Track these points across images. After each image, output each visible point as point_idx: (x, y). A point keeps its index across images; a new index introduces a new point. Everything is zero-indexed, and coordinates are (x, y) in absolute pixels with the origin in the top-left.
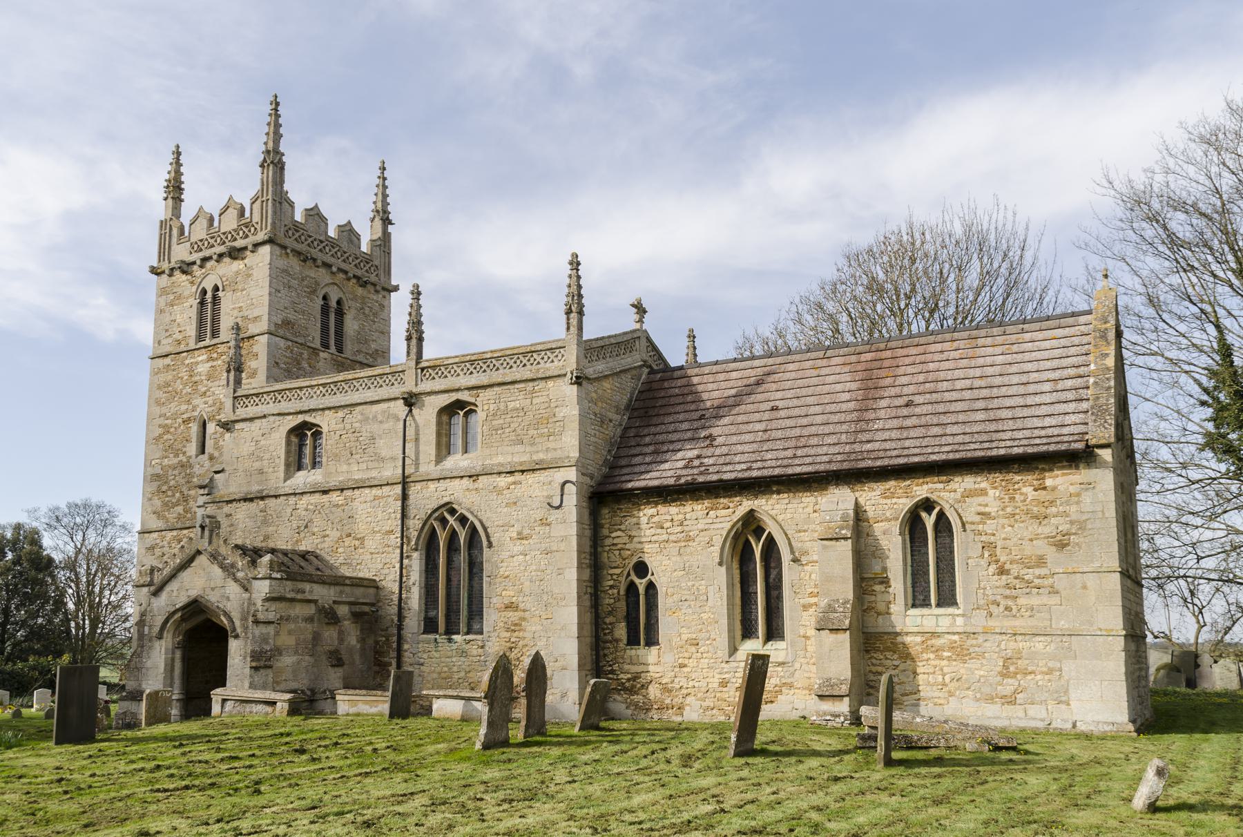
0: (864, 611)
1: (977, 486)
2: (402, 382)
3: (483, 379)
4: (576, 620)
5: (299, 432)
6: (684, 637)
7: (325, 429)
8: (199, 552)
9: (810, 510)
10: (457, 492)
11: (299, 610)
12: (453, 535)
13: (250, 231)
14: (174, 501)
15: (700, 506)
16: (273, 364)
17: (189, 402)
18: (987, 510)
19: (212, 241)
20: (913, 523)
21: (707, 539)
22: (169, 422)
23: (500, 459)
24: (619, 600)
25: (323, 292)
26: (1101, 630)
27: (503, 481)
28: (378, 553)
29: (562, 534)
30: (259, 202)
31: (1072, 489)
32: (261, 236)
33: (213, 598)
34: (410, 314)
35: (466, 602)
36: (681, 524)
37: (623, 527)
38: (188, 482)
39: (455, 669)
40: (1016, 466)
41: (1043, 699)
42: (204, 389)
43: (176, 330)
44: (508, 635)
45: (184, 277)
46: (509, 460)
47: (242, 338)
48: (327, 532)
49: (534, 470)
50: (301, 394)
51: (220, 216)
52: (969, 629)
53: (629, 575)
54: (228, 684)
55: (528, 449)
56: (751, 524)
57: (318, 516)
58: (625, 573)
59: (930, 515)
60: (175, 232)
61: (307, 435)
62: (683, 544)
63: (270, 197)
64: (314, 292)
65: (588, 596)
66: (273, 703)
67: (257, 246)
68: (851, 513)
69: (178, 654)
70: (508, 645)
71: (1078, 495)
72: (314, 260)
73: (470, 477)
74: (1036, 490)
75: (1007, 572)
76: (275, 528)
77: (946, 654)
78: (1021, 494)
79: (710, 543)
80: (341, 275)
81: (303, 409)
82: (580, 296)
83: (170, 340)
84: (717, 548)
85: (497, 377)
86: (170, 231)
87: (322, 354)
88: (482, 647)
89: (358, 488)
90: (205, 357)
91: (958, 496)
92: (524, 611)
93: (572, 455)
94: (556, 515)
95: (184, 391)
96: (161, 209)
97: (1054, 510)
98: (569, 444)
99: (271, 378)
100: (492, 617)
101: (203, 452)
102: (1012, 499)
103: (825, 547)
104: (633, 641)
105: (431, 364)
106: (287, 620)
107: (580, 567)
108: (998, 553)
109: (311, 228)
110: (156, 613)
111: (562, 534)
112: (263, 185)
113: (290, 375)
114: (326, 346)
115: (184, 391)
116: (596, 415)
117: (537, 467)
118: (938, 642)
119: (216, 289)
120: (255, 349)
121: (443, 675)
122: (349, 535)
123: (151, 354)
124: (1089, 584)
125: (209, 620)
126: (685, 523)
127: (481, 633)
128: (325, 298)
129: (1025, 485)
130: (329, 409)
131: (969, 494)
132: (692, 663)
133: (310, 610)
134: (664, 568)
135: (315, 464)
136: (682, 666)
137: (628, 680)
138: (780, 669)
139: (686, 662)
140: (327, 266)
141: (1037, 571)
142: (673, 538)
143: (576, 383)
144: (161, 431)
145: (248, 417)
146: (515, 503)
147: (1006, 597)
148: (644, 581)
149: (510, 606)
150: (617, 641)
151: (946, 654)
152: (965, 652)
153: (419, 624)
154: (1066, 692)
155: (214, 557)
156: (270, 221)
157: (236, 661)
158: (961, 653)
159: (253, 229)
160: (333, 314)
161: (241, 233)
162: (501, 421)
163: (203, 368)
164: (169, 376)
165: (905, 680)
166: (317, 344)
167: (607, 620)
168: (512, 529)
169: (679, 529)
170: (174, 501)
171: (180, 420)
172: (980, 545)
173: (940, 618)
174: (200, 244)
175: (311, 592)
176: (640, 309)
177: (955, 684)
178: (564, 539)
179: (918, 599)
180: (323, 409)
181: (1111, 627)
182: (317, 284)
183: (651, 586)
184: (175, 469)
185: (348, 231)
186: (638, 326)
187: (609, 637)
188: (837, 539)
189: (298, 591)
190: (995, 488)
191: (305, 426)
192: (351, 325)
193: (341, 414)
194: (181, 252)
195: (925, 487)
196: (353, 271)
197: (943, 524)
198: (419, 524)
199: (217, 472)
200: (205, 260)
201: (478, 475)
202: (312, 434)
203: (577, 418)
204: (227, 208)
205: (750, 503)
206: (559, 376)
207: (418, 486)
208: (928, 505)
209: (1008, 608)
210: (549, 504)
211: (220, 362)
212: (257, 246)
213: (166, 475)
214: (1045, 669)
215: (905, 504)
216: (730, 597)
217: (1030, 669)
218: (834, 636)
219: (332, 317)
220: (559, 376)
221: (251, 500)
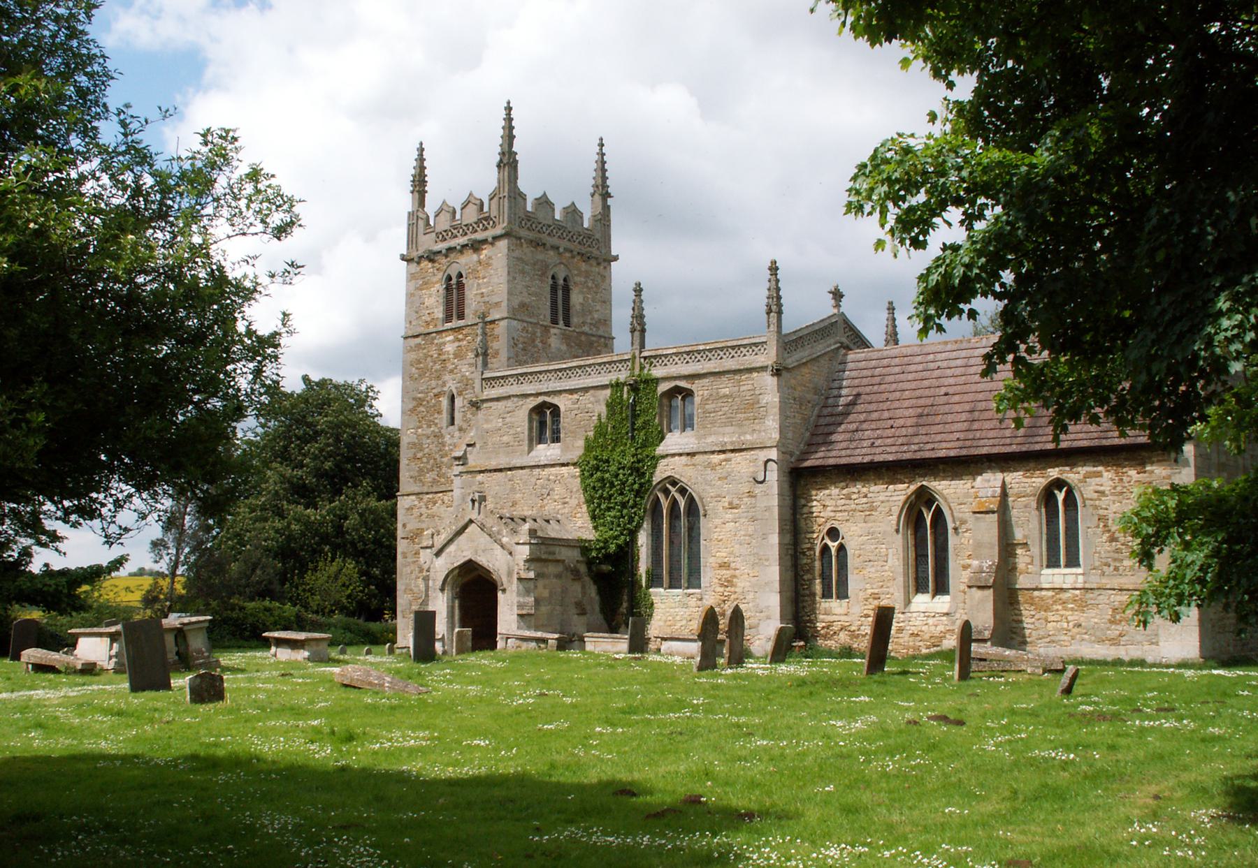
0: (1010, 571)
4: (778, 578)
5: (539, 410)
6: (870, 591)
7: (562, 409)
8: (471, 521)
11: (552, 569)
12: (674, 503)
14: (429, 467)
16: (513, 343)
17: (438, 378)
18: (1102, 488)
19: (455, 232)
20: (1047, 497)
21: (887, 509)
25: (552, 273)
27: (716, 458)
29: (765, 504)
30: (496, 199)
32: (499, 231)
33: (482, 560)
34: (633, 309)
35: (686, 571)
36: (866, 496)
38: (440, 450)
39: (678, 618)
42: (452, 367)
44: (722, 589)
45: (430, 265)
47: (486, 323)
50: (541, 377)
51: (462, 209)
52: (1087, 586)
54: (892, 605)
56: (924, 498)
60: (421, 223)
63: (506, 194)
64: (543, 274)
65: (789, 557)
66: (544, 641)
67: (496, 238)
68: (999, 490)
72: (544, 245)
79: (889, 513)
80: (568, 255)
82: (779, 298)
84: (895, 517)
86: (417, 221)
87: (553, 331)
88: (701, 599)
90: (451, 338)
92: (735, 569)
93: (773, 436)
94: (759, 489)
96: (406, 202)
98: (771, 429)
99: (516, 360)
100: (708, 575)
101: (452, 423)
102: (1121, 480)
103: (977, 519)
104: (827, 594)
105: (653, 353)
107: (782, 532)
109: (541, 216)
112: (499, 182)
114: (554, 321)
116: (795, 399)
118: (1065, 596)
119: (460, 275)
120: (496, 332)
121: (669, 623)
123: (403, 334)
125: (480, 576)
128: (553, 277)
133: (560, 568)
137: (823, 628)
138: (945, 618)
140: (556, 248)
142: (859, 507)
144: (415, 403)
148: (836, 544)
155: (482, 527)
156: (506, 216)
158: (1082, 605)
160: (560, 293)
162: (714, 406)
163: (450, 348)
164: (421, 354)
166: (547, 322)
167: (805, 577)
169: (865, 500)
170: (429, 467)
175: (560, 553)
176: (837, 295)
177: (1076, 630)
178: (768, 509)
179: (1053, 562)
182: (547, 266)
183: (842, 548)
184: (428, 437)
185: (573, 212)
186: (835, 311)
187: (807, 592)
189: (550, 553)
192: (576, 298)
193: (576, 396)
194: (428, 243)
196: (576, 247)
197: (1070, 501)
199: (469, 445)
200: (450, 250)
203: (778, 404)
208: (1059, 484)
209: (1116, 569)
211: (465, 342)
212: (496, 238)
213: (421, 444)
216: (906, 559)
219: (560, 293)
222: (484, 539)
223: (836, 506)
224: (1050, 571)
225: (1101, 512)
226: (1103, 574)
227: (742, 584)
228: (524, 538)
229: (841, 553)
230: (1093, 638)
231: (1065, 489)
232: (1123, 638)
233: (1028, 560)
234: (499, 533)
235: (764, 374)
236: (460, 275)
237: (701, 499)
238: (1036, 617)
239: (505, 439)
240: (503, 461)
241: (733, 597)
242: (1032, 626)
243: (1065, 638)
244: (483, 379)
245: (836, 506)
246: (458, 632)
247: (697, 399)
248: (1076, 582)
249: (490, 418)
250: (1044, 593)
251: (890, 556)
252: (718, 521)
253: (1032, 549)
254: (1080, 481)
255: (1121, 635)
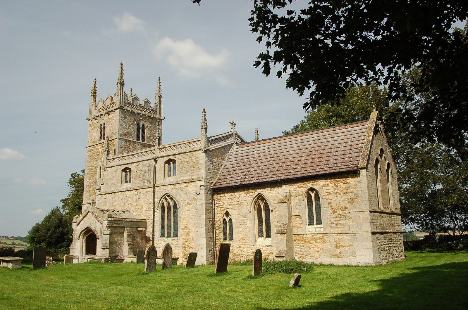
1: (326, 183)
2: (154, 153)
3: (176, 151)
5: (125, 170)
6: (241, 237)
7: (132, 170)
8: (89, 212)
9: (277, 192)
10: (170, 190)
13: (114, 105)
14: (92, 194)
15: (244, 192)
17: (96, 161)
21: (247, 203)
22: (91, 168)
23: (182, 178)
24: (221, 225)
26: (364, 231)
27: (183, 186)
28: (147, 211)
31: (354, 183)
32: (117, 107)
33: (92, 227)
36: (238, 199)
37: (221, 200)
40: (337, 176)
41: (348, 255)
42: (100, 157)
43: (93, 138)
46: (185, 178)
48: (133, 204)
49: (192, 182)
53: (223, 216)
55: (191, 174)
56: (260, 197)
57: (130, 198)
58: (222, 216)
59: (313, 193)
61: (127, 171)
62: (239, 205)
69: (84, 244)
70: (185, 241)
71: (357, 185)
73: (173, 184)
74: (344, 184)
75: (336, 212)
76: (118, 203)
77: (318, 241)
78: (340, 185)
81: (126, 163)
83: (91, 141)
85: (181, 151)
88: (177, 241)
89: (141, 189)
91: (320, 186)
95: (95, 158)
97: (349, 190)
101: (100, 178)
103: (279, 206)
106: (114, 233)
108: (333, 206)
110: (78, 231)
111: (200, 203)
113: (126, 151)
114: (138, 139)
115: (95, 158)
117: (193, 181)
118: (315, 237)
119: (104, 124)
122: (139, 205)
124: (360, 215)
126: (240, 198)
127: (177, 237)
129: (340, 182)
130: (133, 163)
131: (323, 186)
132: (242, 246)
134: (234, 214)
135: (174, 174)
136: (240, 247)
138: (269, 247)
139: (241, 246)
141: (345, 212)
142: (236, 203)
143: (204, 152)
144: (89, 171)
145: (110, 166)
146: (186, 193)
147: (336, 221)
148: (228, 218)
149: (186, 228)
150: (220, 239)
151: (318, 241)
152: (324, 240)
153: (159, 234)
154: (355, 253)
157: (99, 246)
158: (323, 240)
159: (114, 104)
160: (140, 129)
161: (111, 106)
163: (100, 150)
165: (306, 250)
168: (186, 202)
169: (238, 200)
171: (94, 167)
172: (328, 203)
173: (316, 229)
174: (100, 109)
178: (201, 204)
179: (311, 223)
180: (131, 163)
181: (367, 230)
183: (230, 220)
188: (283, 203)
190: (331, 184)
191: (127, 168)
193: (136, 164)
195: (311, 184)
197: (317, 197)
198: (158, 200)
199: (102, 185)
200: (102, 115)
201: (175, 184)
202: (129, 171)
204: (108, 98)
205: (259, 191)
206: (199, 150)
207: (158, 188)
210: (196, 193)
214: (348, 245)
215: (305, 190)
217: (344, 245)
218: (282, 236)
220: (199, 150)
221: (111, 193)
222: (93, 219)
223: (228, 203)
224: (310, 227)
225: (329, 201)
226: (331, 227)
227: (192, 235)
228: (106, 217)
229: (230, 222)
230: (329, 255)
231: (315, 192)
232: (341, 254)
233: (301, 222)
234: (98, 216)
235: (201, 151)
236: (104, 124)
237: (178, 202)
238: (305, 246)
239: (114, 182)
240: (112, 190)
241: (189, 240)
242: (304, 250)
243: (317, 255)
244: (107, 160)
245: (228, 203)
246: (66, 257)
247: (177, 163)
248: (320, 231)
249: (108, 174)
250: (308, 236)
251: (248, 223)
252: (183, 210)
253: (302, 217)
254: (320, 188)
255: (340, 253)
